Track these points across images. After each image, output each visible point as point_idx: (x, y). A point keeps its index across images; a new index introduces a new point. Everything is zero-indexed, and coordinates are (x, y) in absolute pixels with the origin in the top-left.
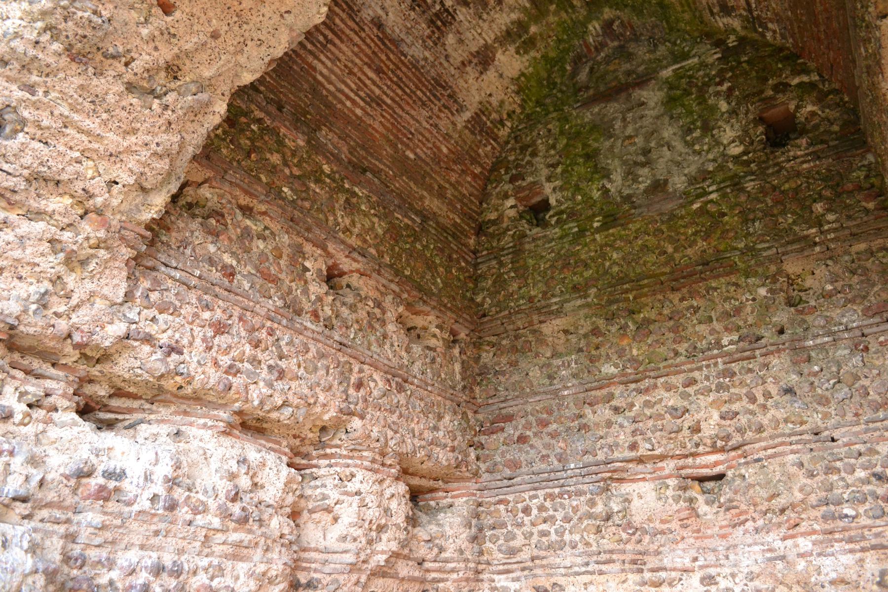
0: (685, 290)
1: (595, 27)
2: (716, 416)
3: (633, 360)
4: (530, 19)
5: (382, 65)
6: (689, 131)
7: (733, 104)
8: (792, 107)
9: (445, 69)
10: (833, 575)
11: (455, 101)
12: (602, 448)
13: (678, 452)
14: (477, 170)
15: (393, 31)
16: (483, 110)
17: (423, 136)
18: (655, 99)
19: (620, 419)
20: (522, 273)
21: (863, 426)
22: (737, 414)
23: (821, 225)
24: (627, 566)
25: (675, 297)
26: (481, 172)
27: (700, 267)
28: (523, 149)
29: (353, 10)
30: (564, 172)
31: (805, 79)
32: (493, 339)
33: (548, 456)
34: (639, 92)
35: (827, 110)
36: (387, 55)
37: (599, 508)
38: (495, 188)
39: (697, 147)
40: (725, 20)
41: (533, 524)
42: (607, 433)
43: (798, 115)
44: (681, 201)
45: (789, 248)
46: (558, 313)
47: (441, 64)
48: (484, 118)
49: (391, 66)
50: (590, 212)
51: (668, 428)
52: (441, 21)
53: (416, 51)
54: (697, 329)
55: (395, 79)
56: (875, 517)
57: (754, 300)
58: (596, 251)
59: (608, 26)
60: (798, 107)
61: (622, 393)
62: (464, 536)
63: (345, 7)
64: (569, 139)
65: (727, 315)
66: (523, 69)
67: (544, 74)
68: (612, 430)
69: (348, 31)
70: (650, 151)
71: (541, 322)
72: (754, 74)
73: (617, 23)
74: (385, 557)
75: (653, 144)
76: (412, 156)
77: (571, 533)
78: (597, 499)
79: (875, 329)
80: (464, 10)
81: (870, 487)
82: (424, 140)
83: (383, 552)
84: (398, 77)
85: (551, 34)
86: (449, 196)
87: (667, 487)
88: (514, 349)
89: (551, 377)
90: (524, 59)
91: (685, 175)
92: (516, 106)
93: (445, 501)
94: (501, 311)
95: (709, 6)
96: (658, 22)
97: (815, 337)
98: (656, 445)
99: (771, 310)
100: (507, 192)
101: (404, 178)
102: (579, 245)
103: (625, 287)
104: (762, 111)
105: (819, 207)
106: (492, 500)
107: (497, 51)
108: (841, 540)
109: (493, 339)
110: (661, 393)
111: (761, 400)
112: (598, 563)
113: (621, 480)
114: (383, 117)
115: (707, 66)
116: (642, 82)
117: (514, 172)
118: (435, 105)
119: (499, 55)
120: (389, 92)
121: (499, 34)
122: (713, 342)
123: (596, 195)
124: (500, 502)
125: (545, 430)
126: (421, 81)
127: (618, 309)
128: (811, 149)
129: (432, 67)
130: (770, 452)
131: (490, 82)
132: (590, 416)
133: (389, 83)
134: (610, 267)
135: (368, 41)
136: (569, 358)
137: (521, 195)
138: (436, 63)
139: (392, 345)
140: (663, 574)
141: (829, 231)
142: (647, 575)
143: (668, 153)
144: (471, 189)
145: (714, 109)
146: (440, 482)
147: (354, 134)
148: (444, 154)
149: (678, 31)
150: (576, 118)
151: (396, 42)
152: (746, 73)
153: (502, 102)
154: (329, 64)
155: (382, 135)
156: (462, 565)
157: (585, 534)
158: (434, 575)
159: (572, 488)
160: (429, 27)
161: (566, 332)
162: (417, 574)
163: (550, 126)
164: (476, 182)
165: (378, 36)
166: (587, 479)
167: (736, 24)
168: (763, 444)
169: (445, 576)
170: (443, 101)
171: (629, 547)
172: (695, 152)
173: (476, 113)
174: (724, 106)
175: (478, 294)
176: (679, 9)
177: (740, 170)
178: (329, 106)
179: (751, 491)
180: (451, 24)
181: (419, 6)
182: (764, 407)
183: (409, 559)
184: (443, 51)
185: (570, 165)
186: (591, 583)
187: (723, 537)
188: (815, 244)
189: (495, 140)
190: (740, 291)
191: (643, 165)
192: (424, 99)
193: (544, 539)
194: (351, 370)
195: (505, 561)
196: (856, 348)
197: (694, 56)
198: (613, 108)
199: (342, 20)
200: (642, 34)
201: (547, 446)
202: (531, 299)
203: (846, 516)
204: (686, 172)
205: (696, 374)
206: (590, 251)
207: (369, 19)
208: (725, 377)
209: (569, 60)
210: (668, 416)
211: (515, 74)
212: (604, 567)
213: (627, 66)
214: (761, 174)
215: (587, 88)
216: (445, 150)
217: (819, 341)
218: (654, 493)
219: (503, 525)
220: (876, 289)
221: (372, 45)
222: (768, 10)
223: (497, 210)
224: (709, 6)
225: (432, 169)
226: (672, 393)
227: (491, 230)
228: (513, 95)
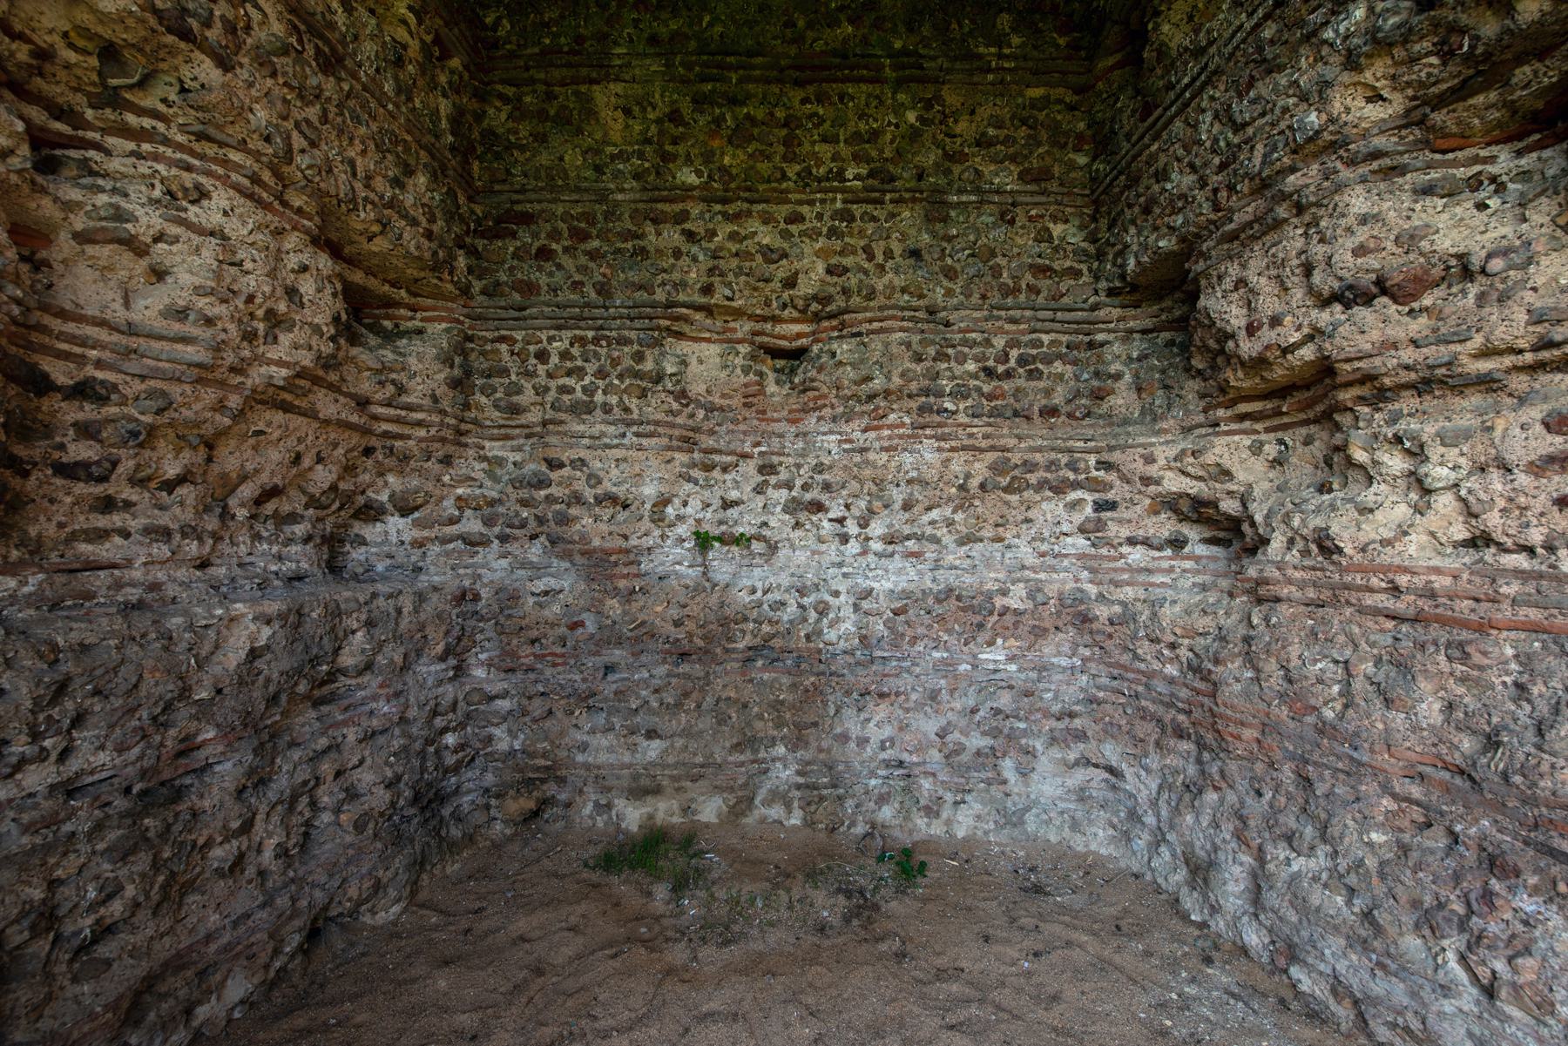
0: (811, 89)
2: (820, 268)
3: (724, 170)
10: (914, 474)
12: (663, 284)
13: (758, 312)
19: (695, 249)
21: (986, 313)
22: (846, 270)
23: (1000, 48)
24: (675, 443)
25: (796, 95)
32: (510, 91)
33: (582, 283)
37: (648, 365)
41: (550, 375)
42: (673, 265)
45: (958, 65)
51: (758, 273)
56: (974, 416)
57: (897, 126)
61: (702, 213)
62: (442, 376)
65: (857, 137)
68: (680, 263)
74: (284, 372)
77: (605, 393)
78: (648, 353)
79: (1028, 199)
81: (977, 383)
83: (280, 363)
87: (738, 353)
88: (542, 115)
89: (598, 169)
93: (410, 324)
97: (960, 192)
98: (737, 295)
106: (489, 335)
108: (931, 437)
110: (754, 225)
111: (880, 258)
112: (637, 435)
113: (680, 335)
124: (502, 339)
125: (583, 246)
127: (713, 91)
130: (876, 325)
132: (652, 238)
140: (717, 458)
141: (1007, 57)
142: (696, 455)
146: (403, 293)
156: (436, 418)
157: (625, 397)
158: (385, 427)
159: (614, 334)
162: (354, 418)
166: (638, 324)
168: (868, 315)
169: (406, 431)
171: (679, 420)
179: (841, 370)
182: (882, 268)
183: (338, 390)
186: (625, 460)
187: (793, 422)
188: (989, 70)
193: (566, 398)
195: (502, 422)
196: (1002, 219)
201: (582, 269)
203: (946, 410)
205: (805, 209)
208: (842, 220)
210: (759, 258)
212: (645, 442)
217: (964, 198)
218: (718, 360)
219: (505, 372)
220: (1041, 150)
226: (770, 228)
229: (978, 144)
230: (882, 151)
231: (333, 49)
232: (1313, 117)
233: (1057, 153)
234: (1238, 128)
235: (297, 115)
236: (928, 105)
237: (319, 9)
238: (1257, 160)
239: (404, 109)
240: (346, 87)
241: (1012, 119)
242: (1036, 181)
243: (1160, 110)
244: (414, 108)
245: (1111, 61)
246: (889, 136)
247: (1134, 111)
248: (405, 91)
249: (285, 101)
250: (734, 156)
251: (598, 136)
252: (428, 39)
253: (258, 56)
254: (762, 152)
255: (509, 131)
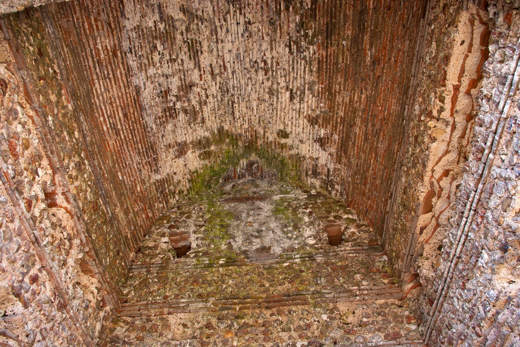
0: (274, 310)
1: (243, 162)
4: (213, 140)
5: (129, 114)
6: (286, 226)
7: (312, 219)
8: (343, 228)
9: (159, 142)
11: (156, 164)
14: (150, 215)
15: (144, 101)
16: (168, 180)
17: (131, 171)
18: (268, 208)
20: (163, 281)
25: (268, 313)
26: (151, 217)
27: (286, 298)
28: (182, 214)
29: (129, 73)
30: (205, 231)
31: (351, 217)
32: (129, 319)
34: (259, 202)
35: (362, 233)
36: (134, 111)
38: (158, 229)
39: (290, 235)
40: (312, 180)
43: (346, 233)
44: (277, 260)
45: (341, 295)
46: (184, 310)
47: (158, 137)
48: (166, 186)
49: (133, 119)
50: (219, 255)
52: (170, 113)
53: (150, 121)
54: (280, 334)
55: (131, 128)
57: (318, 322)
58: (218, 277)
59: (251, 164)
60: (346, 228)
63: (126, 68)
64: (212, 215)
65: (299, 328)
66: (198, 168)
67: (207, 178)
69: (121, 82)
70: (262, 231)
71: (169, 313)
72: (324, 209)
73: (255, 165)
75: (263, 228)
76: (121, 178)
80: (183, 115)
82: (131, 174)
84: (133, 127)
85: (220, 155)
86: (130, 217)
88: (143, 329)
90: (201, 163)
91: (281, 247)
92: (186, 189)
94: (140, 301)
95: (307, 169)
96: (277, 173)
99: (329, 329)
100: (165, 233)
101: (111, 185)
102: (207, 271)
103: (235, 301)
104: (327, 226)
105: (358, 277)
107: (190, 149)
109: (129, 319)
114: (116, 142)
115: (299, 199)
116: (262, 198)
117: (173, 223)
118: (145, 159)
119: (189, 153)
120: (125, 131)
121: (195, 140)
122: (291, 344)
123: (224, 247)
126: (144, 140)
127: (228, 313)
128: (354, 248)
129: (153, 135)
131: (178, 166)
133: (127, 127)
134: (226, 288)
135: (128, 96)
136: (185, 341)
137: (174, 238)
138: (156, 135)
139: (67, 273)
143: (272, 235)
144: (142, 223)
145: (301, 219)
147: (97, 137)
148: (137, 191)
149: (285, 181)
150: (219, 206)
151: (142, 108)
152: (319, 208)
153: (179, 181)
154: (103, 90)
155: (110, 151)
160: (162, 112)
161: (185, 326)
163: (201, 207)
164: (147, 221)
165: (134, 97)
167: (317, 183)
170: (150, 160)
172: (288, 237)
173: (163, 179)
174: (306, 219)
175: (126, 287)
176: (291, 167)
177: (313, 251)
178: (92, 110)
180: (174, 118)
181: (162, 97)
184: (163, 131)
185: (210, 228)
188: (356, 295)
189: (166, 203)
190: (310, 315)
191: (257, 237)
192: (141, 150)
194: (34, 264)
197: (293, 194)
198: (242, 207)
199: (121, 73)
200: (265, 177)
202: (166, 297)
204: (282, 246)
206: (214, 276)
207: (135, 84)
209: (222, 177)
211: (193, 169)
213: (255, 190)
214: (326, 253)
215: (229, 194)
216: (139, 189)
220: (392, 325)
221: (129, 99)
222: (338, 177)
223: (155, 241)
224: (307, 169)
225: (127, 193)
227: (147, 252)
228: (187, 181)
229: (360, 326)
230: (313, 333)
231: (65, 302)
232: (492, 292)
233: (400, 326)
234: (469, 301)
235: (43, 326)
236: (332, 311)
237: (65, 287)
238: (482, 312)
239: (83, 326)
240: (64, 316)
241: (373, 313)
242: (394, 339)
243: (436, 301)
244: (87, 326)
245: (410, 286)
246: (315, 327)
247: (426, 303)
248: (86, 319)
249: (41, 321)
250: (238, 341)
251: (170, 337)
252: (100, 299)
253: (38, 303)
254: (252, 338)
255: (125, 337)
